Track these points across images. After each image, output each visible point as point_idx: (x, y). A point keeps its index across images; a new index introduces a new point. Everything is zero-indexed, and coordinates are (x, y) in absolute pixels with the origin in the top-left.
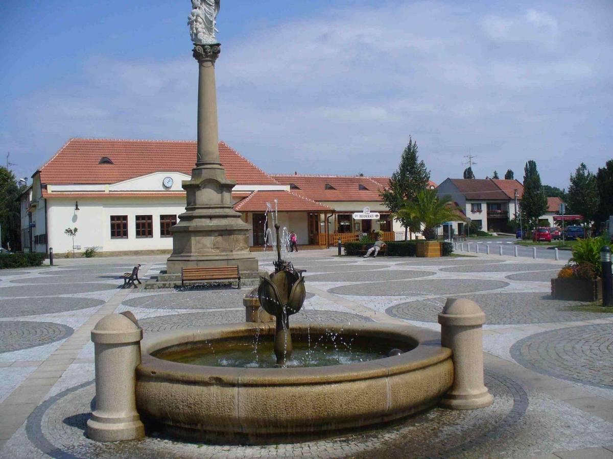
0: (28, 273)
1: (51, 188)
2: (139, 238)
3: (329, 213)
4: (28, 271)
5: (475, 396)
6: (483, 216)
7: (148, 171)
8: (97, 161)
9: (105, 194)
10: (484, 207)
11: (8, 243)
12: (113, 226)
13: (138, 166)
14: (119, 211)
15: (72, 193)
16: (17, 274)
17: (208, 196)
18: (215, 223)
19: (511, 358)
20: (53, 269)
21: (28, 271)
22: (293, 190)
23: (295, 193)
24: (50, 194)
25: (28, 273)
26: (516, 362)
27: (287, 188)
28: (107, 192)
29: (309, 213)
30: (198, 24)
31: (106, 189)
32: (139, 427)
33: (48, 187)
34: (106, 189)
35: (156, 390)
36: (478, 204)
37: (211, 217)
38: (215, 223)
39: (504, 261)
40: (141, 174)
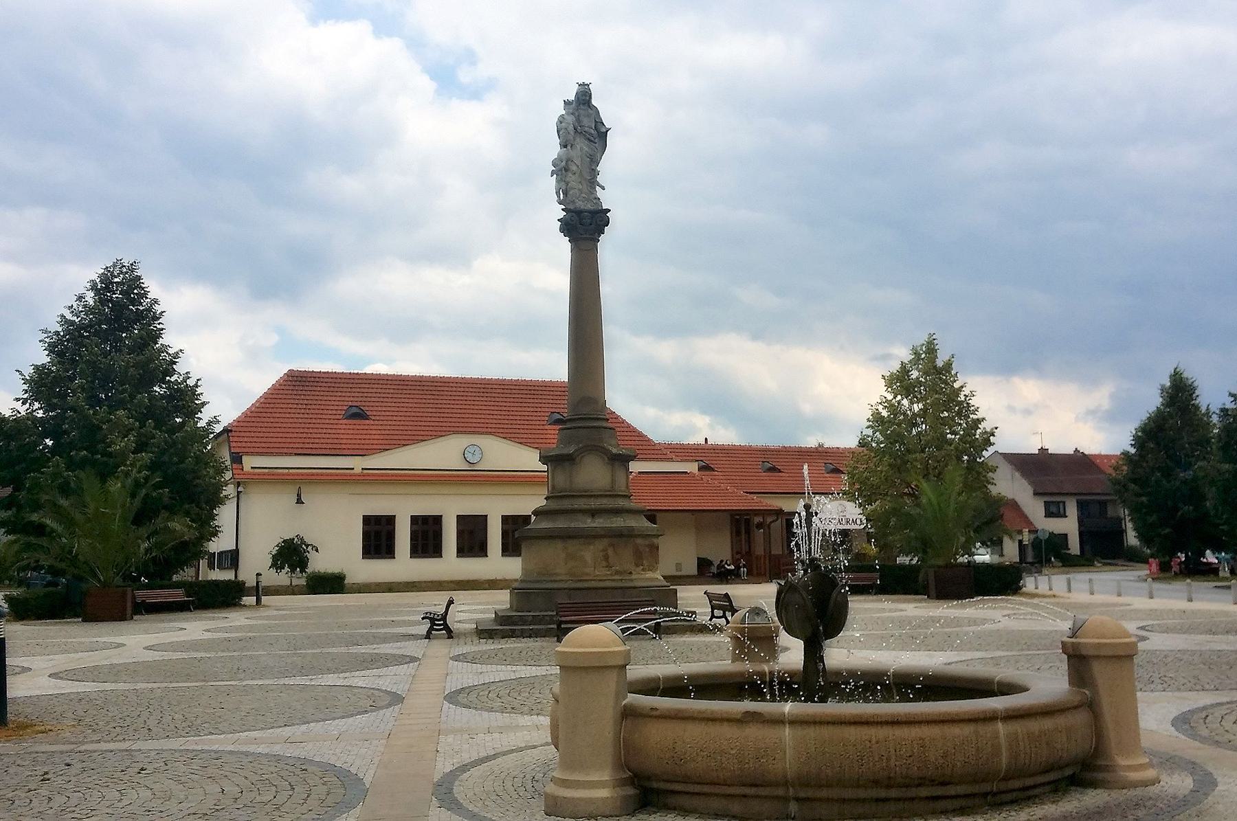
0: (182, 629)
1: (249, 462)
2: (415, 557)
3: (770, 514)
4: (119, 640)
5: (1130, 768)
6: (1069, 525)
7: (417, 437)
8: (339, 412)
9: (355, 475)
10: (1072, 510)
11: (806, 467)
12: (366, 536)
13: (437, 424)
14: (380, 505)
15: (291, 471)
16: (213, 619)
17: (593, 474)
18: (599, 523)
19: (1177, 733)
20: (262, 612)
21: (119, 640)
22: (703, 473)
23: (707, 476)
24: (249, 474)
25: (182, 629)
26: (1186, 738)
27: (692, 468)
28: (358, 470)
29: (732, 516)
30: (570, 175)
31: (357, 464)
32: (630, 796)
33: (245, 459)
34: (357, 464)
35: (657, 737)
36: (1059, 502)
37: (594, 513)
38: (599, 523)
39: (1129, 605)
40: (439, 433)
